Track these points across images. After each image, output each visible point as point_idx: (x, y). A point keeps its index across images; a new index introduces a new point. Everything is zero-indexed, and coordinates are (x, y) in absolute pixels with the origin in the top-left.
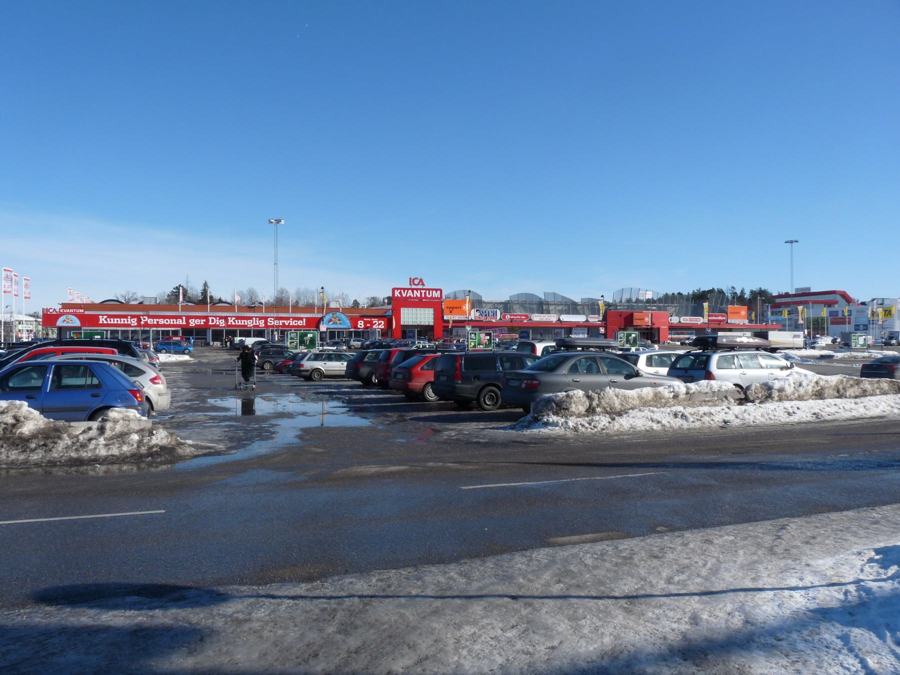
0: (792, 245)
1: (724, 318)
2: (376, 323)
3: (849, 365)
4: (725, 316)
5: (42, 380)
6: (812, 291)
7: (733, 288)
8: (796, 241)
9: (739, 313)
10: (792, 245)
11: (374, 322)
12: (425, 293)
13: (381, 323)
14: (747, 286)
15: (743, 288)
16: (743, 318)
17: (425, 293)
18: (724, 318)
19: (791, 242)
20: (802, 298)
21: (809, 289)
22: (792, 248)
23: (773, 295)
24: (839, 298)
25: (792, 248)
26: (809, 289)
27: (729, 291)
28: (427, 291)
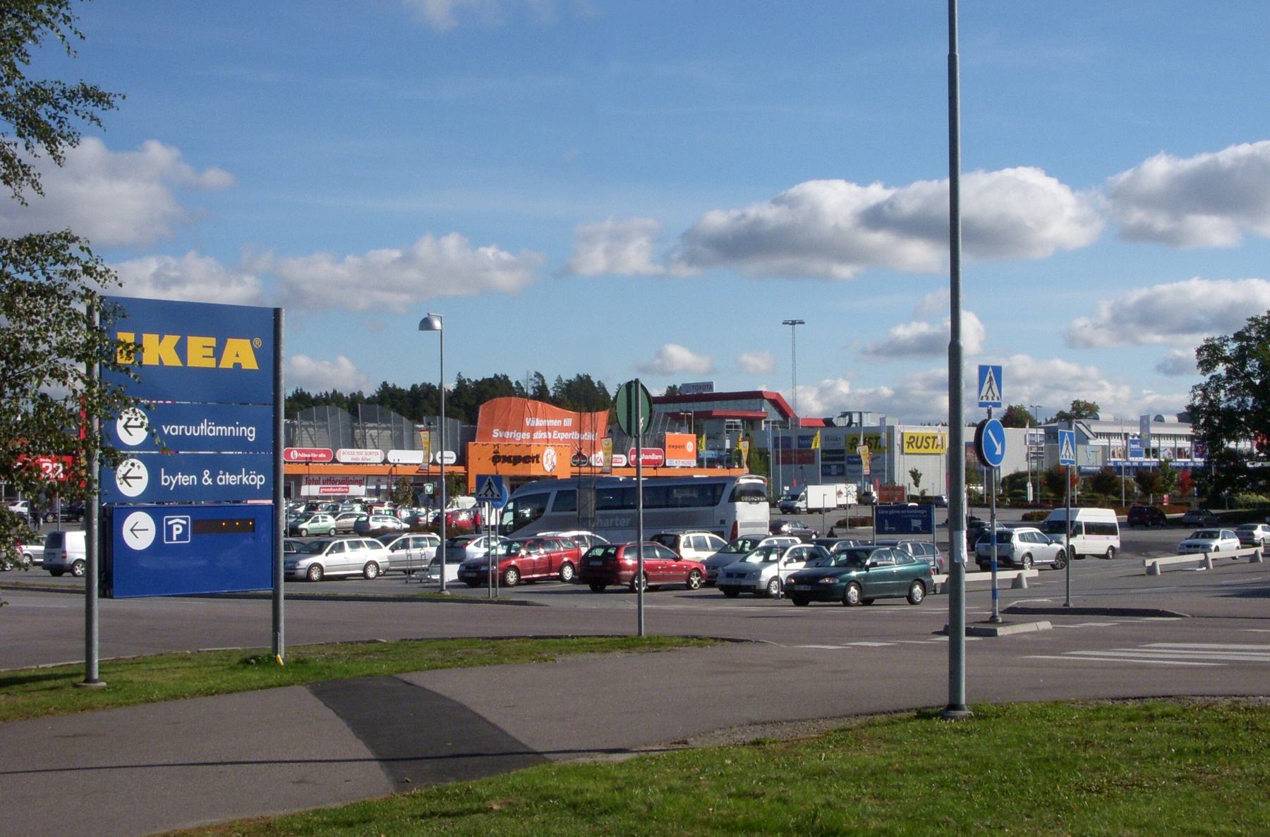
0: (793, 330)
1: (660, 457)
2: (47, 468)
3: (887, 512)
4: (660, 454)
5: (83, 533)
6: (716, 390)
7: (538, 375)
8: (802, 323)
9: (683, 446)
10: (793, 330)
11: (44, 465)
13: (58, 468)
14: (558, 372)
15: (459, 375)
16: (689, 456)
18: (660, 457)
19: (793, 323)
20: (1110, 427)
21: (710, 386)
22: (793, 334)
23: (243, 367)
24: (766, 407)
25: (793, 334)
26: (710, 386)
27: (531, 383)
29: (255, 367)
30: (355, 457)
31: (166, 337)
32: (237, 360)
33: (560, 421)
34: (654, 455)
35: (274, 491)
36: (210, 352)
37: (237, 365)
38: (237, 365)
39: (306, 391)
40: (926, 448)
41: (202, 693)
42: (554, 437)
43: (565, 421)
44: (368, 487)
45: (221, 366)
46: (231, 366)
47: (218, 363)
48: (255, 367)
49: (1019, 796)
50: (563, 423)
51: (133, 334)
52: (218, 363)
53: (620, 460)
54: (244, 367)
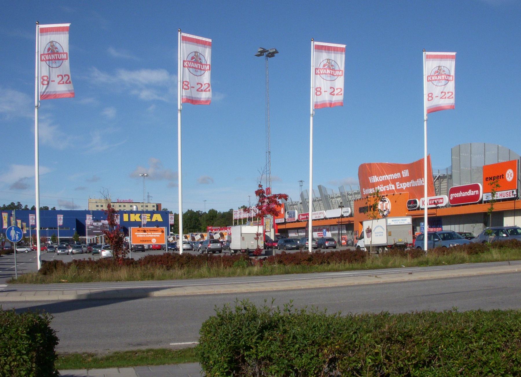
8: (327, 91)
9: (503, 176)
12: (57, 56)
17: (57, 56)
28: (58, 55)
29: (161, 220)
30: (317, 216)
31: (137, 214)
32: (157, 219)
33: (399, 174)
34: (470, 191)
35: (502, 201)
36: (149, 217)
37: (157, 221)
38: (157, 221)
39: (215, 209)
40: (507, 192)
41: (503, 314)
42: (398, 188)
43: (403, 172)
44: (332, 233)
45: (152, 221)
46: (155, 221)
47: (151, 220)
48: (161, 220)
49: (284, 352)
50: (401, 175)
51: (124, 220)
52: (151, 220)
53: (441, 201)
54: (158, 221)
